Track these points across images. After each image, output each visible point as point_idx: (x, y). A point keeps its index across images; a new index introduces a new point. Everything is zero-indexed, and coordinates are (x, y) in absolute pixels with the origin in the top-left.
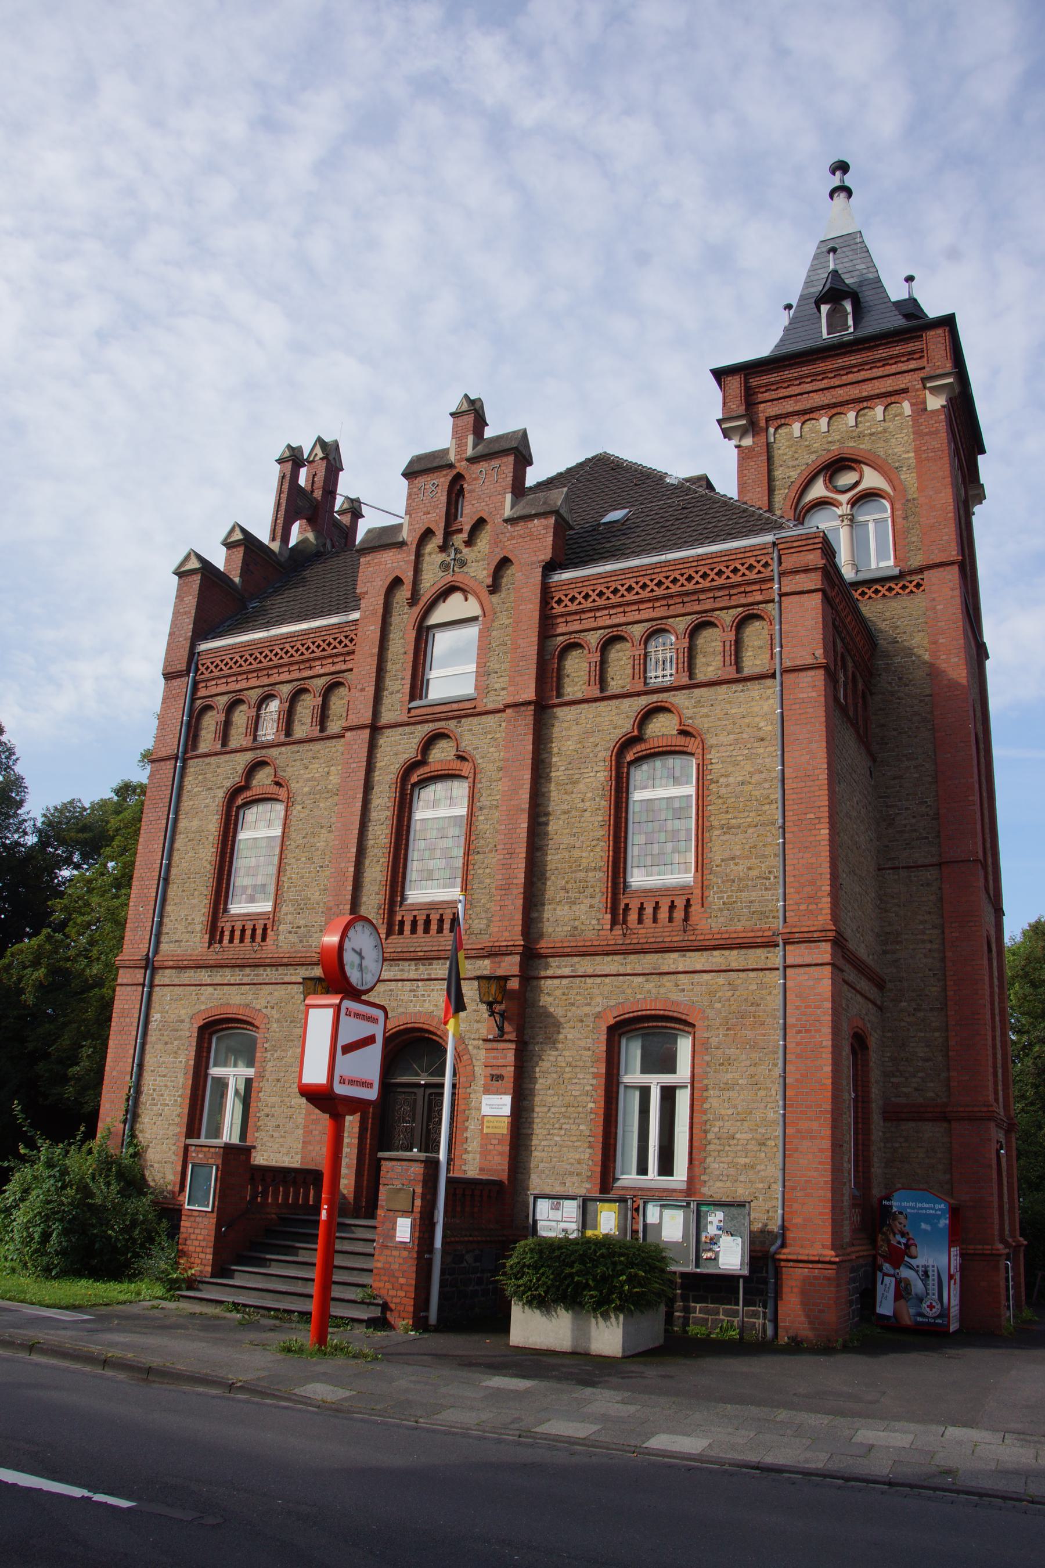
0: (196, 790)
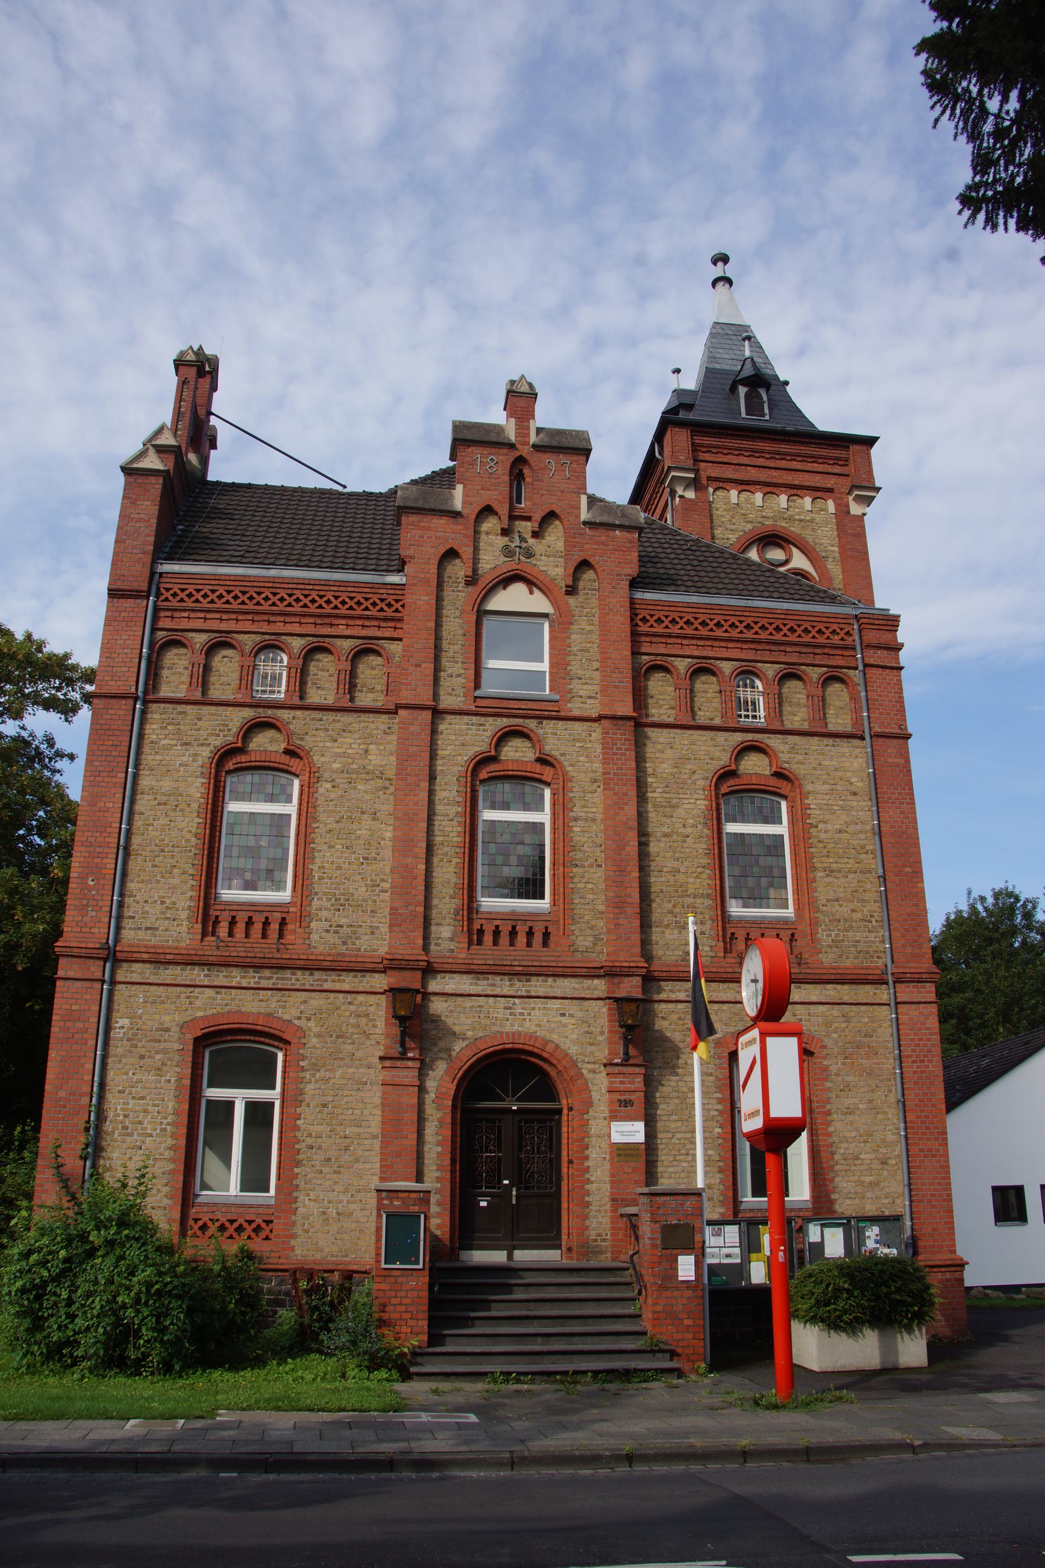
0: (165, 742)
